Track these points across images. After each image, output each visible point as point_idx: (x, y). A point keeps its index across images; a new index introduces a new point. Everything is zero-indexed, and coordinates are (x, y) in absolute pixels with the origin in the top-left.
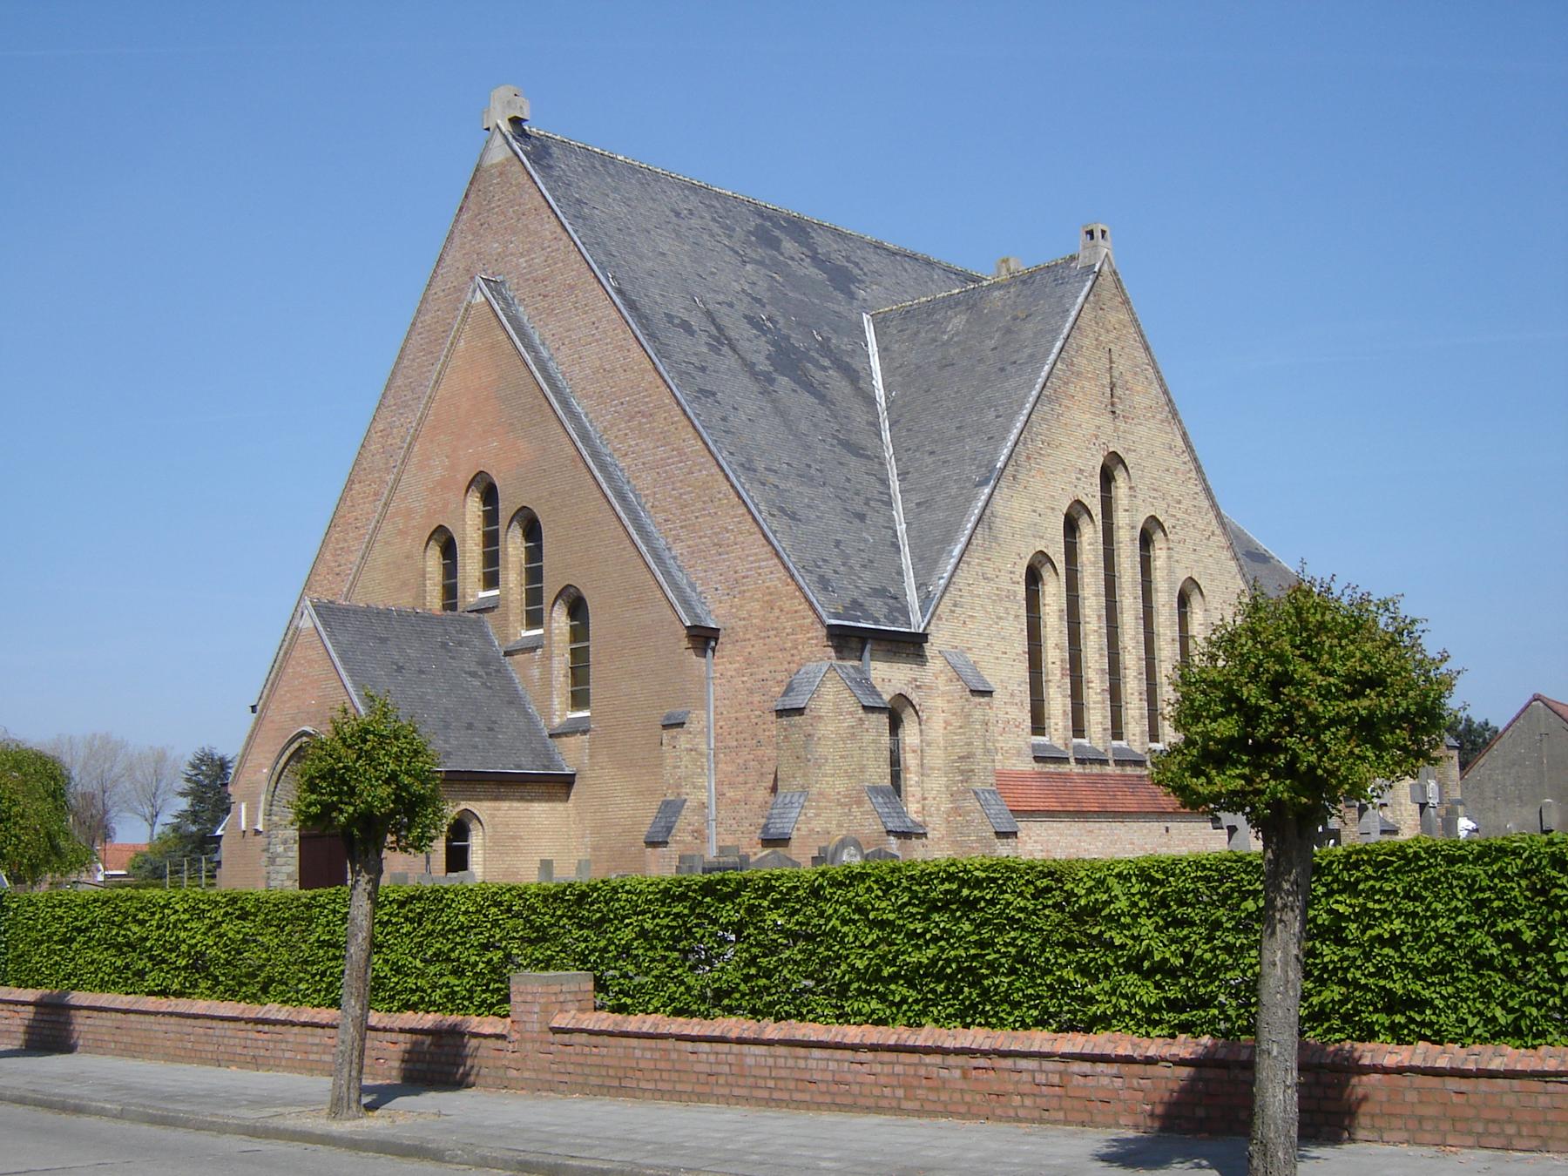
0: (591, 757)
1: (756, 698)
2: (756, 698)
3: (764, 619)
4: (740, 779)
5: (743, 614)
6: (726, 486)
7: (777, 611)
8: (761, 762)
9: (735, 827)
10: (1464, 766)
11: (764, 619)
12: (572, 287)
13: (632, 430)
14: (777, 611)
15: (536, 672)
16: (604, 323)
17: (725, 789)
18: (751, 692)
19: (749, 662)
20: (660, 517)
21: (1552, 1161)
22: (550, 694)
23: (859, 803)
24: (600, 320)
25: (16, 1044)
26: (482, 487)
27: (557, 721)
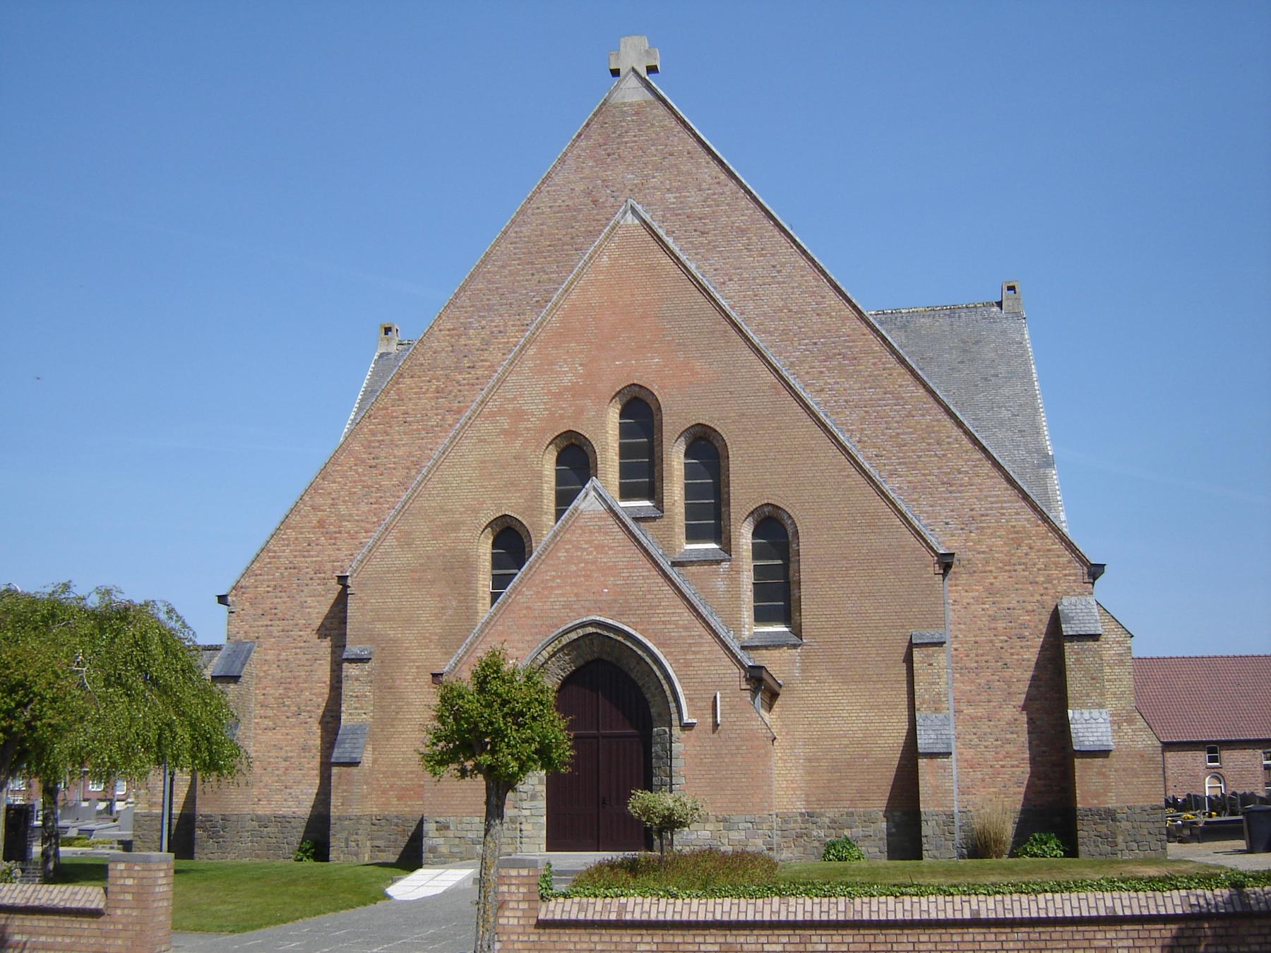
0: (803, 671)
1: (1000, 625)
2: (1000, 625)
3: (1009, 554)
4: (984, 697)
5: (984, 548)
6: (957, 432)
7: (1025, 549)
8: (1009, 683)
9: (976, 741)
10: (682, 824)
11: (1009, 554)
12: (742, 231)
13: (829, 369)
14: (1025, 549)
15: (721, 585)
16: (788, 269)
17: (963, 706)
18: (994, 619)
19: (991, 591)
20: (872, 452)
21: (34, 581)
22: (739, 607)
23: (1130, 721)
24: (783, 265)
25: (393, 858)
26: (625, 400)
27: (746, 634)
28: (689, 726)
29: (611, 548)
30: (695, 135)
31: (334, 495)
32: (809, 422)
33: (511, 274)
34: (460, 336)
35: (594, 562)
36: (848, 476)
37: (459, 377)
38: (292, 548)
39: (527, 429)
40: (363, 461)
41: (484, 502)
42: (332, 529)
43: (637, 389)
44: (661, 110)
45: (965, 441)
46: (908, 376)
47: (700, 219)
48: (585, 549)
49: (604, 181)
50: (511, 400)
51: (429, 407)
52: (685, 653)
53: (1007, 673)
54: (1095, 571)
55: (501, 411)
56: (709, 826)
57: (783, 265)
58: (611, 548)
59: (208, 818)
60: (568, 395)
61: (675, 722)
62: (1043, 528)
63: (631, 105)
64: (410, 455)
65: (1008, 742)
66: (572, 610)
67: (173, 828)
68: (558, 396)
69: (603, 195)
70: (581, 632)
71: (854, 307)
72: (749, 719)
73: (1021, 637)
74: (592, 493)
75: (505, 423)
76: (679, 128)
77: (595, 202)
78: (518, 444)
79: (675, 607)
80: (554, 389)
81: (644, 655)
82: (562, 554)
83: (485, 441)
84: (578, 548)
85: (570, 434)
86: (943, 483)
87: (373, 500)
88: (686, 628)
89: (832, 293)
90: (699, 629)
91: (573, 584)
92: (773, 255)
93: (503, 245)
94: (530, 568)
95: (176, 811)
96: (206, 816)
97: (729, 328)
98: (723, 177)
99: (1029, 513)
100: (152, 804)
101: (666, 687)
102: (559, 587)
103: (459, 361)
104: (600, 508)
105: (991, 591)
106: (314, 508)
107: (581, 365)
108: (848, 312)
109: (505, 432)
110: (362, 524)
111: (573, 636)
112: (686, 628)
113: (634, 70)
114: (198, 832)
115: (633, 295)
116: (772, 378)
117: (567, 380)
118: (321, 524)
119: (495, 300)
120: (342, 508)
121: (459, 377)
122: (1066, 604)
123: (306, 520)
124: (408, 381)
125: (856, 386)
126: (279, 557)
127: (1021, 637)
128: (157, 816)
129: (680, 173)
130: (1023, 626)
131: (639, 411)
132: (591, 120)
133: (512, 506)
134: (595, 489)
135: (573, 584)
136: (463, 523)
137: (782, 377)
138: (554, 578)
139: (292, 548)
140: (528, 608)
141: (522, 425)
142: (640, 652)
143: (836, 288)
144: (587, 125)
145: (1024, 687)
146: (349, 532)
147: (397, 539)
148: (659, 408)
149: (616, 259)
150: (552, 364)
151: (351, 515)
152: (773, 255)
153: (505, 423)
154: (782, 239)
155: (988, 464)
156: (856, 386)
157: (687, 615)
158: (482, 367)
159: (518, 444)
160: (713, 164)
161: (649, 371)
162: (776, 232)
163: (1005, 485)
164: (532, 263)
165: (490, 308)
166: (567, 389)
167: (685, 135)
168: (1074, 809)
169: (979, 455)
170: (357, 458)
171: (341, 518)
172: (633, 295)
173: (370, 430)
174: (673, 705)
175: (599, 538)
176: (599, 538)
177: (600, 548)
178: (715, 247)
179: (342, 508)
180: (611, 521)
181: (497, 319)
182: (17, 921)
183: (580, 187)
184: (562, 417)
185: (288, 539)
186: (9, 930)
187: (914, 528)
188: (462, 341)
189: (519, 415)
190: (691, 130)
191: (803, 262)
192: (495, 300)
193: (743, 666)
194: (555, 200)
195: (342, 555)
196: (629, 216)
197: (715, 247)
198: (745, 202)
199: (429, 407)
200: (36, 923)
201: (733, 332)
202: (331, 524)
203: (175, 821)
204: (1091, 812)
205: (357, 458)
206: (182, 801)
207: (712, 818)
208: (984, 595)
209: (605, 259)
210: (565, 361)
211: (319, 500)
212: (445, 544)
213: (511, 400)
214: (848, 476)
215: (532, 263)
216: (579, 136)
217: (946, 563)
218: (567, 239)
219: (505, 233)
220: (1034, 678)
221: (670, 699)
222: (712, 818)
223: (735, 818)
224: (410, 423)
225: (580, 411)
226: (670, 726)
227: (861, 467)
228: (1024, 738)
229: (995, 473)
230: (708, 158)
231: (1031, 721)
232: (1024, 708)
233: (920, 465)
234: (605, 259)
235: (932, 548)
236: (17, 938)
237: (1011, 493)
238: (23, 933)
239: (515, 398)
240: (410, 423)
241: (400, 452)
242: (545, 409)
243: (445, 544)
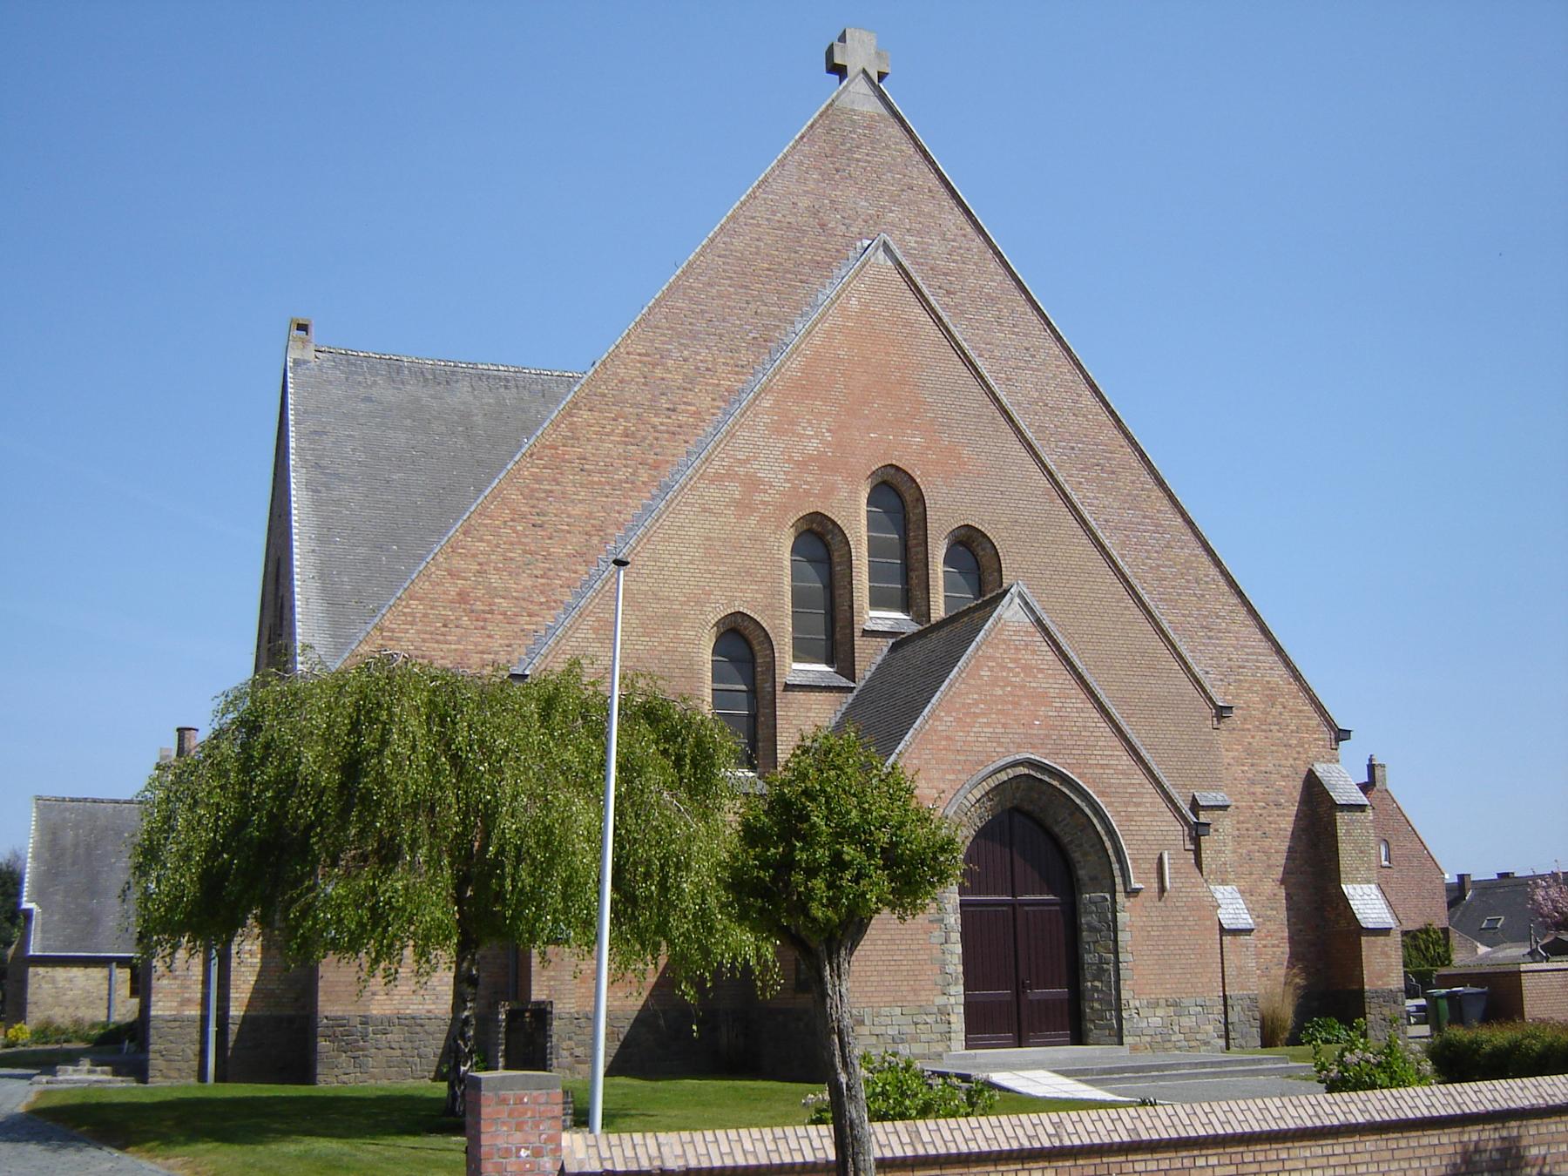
2: (1259, 789)
12: (993, 300)
19: (1250, 752)
24: (1037, 349)
28: (1137, 891)
29: (1041, 671)
30: (937, 170)
31: (481, 558)
32: (1085, 540)
33: (720, 296)
34: (655, 365)
35: (1023, 687)
36: (1126, 608)
37: (656, 420)
38: (419, 626)
39: (763, 503)
40: (523, 516)
41: (710, 593)
42: (479, 606)
43: (893, 471)
44: (896, 130)
45: (1222, 582)
46: (1166, 501)
47: (945, 274)
48: (1011, 669)
49: (832, 202)
50: (742, 463)
51: (615, 454)
52: (1126, 804)
53: (1267, 843)
54: (1342, 735)
55: (730, 475)
56: (1160, 1012)
57: (1037, 349)
58: (1041, 671)
59: (338, 1022)
60: (814, 466)
61: (1119, 888)
62: (1295, 687)
63: (863, 115)
64: (590, 516)
65: (1269, 919)
66: (1000, 744)
67: (232, 1038)
68: (802, 465)
69: (833, 220)
70: (1011, 773)
71: (1112, 413)
72: (1194, 885)
73: (1278, 805)
74: (1017, 600)
75: (735, 490)
76: (918, 157)
77: (822, 226)
78: (753, 521)
79: (1113, 748)
80: (797, 457)
81: (1083, 805)
82: (985, 673)
83: (710, 511)
84: (1004, 668)
85: (817, 517)
86: (1203, 627)
87: (540, 572)
88: (1124, 773)
89: (1088, 393)
90: (1139, 777)
91: (1000, 712)
92: (1025, 335)
93: (710, 257)
94: (951, 686)
95: (236, 1011)
96: (336, 1018)
97: (998, 414)
98: (969, 229)
99: (1281, 670)
100: (185, 1002)
101: (1108, 844)
102: (983, 714)
103: (654, 399)
104: (1025, 619)
105: (1250, 752)
106: (452, 574)
107: (829, 430)
108: (1105, 417)
109: (738, 504)
110: (524, 604)
111: (1003, 777)
112: (1124, 773)
113: (864, 71)
114: (323, 1044)
115: (887, 353)
116: (1044, 482)
117: (813, 446)
118: (463, 597)
119: (701, 326)
120: (494, 578)
121: (656, 420)
122: (1320, 769)
123: (439, 589)
124: (586, 415)
125: (1116, 505)
126: (399, 640)
127: (1278, 805)
128: (190, 1019)
129: (920, 213)
130: (1279, 793)
131: (896, 496)
132: (815, 122)
133: (746, 601)
134: (1021, 595)
135: (1000, 712)
136: (686, 616)
137: (1057, 483)
138: (976, 703)
139: (419, 626)
140: (948, 738)
141: (758, 498)
142: (1078, 801)
143: (1093, 387)
144: (812, 126)
145: (1281, 859)
146: (504, 614)
147: (596, 631)
148: (920, 499)
149: (867, 305)
150: (792, 423)
151: (506, 589)
152: (1025, 335)
153: (735, 490)
154: (1035, 318)
155: (1244, 611)
156: (1116, 505)
157: (1126, 760)
158: (686, 411)
159: (753, 521)
160: (957, 211)
161: (910, 451)
162: (1028, 308)
163: (1260, 636)
164: (746, 287)
165: (694, 336)
166: (812, 459)
167: (925, 168)
168: (1362, 990)
169: (1235, 600)
170: (513, 511)
171: (492, 592)
172: (887, 353)
173: (532, 474)
174: (1116, 866)
175: (1026, 656)
176: (1026, 656)
177: (1027, 669)
178: (963, 312)
179: (494, 578)
180: (1038, 637)
181: (704, 352)
182: (1532, 1128)
183: (804, 203)
184: (807, 493)
185: (412, 614)
186: (1524, 1142)
187: (1193, 675)
188: (658, 372)
189: (753, 484)
190: (933, 163)
191: (1057, 350)
192: (701, 326)
193: (1187, 822)
194: (774, 213)
195: (495, 644)
196: (881, 254)
197: (963, 312)
198: (994, 265)
199: (615, 454)
200: (1553, 1128)
201: (1002, 420)
202: (478, 599)
203: (233, 1029)
204: (1377, 994)
205: (513, 511)
206: (246, 996)
207: (1162, 1002)
208: (1244, 755)
209: (854, 301)
210: (809, 421)
211: (458, 563)
212: (661, 643)
213: (742, 463)
214: (1126, 608)
215: (746, 287)
216: (802, 137)
217: (1222, 712)
218: (789, 265)
219: (712, 240)
220: (1291, 850)
221: (1113, 859)
222: (1162, 1002)
223: (1186, 1002)
224: (589, 473)
225: (829, 490)
226: (1114, 893)
227: (1140, 599)
228: (1283, 915)
229: (1250, 622)
230: (952, 203)
231: (1289, 897)
232: (1283, 882)
233: (1180, 604)
234: (854, 301)
235: (1210, 699)
236: (1534, 1151)
237: (1265, 645)
238: (1539, 1145)
239: (747, 461)
240: (589, 473)
241: (576, 511)
242: (787, 481)
243: (661, 643)
